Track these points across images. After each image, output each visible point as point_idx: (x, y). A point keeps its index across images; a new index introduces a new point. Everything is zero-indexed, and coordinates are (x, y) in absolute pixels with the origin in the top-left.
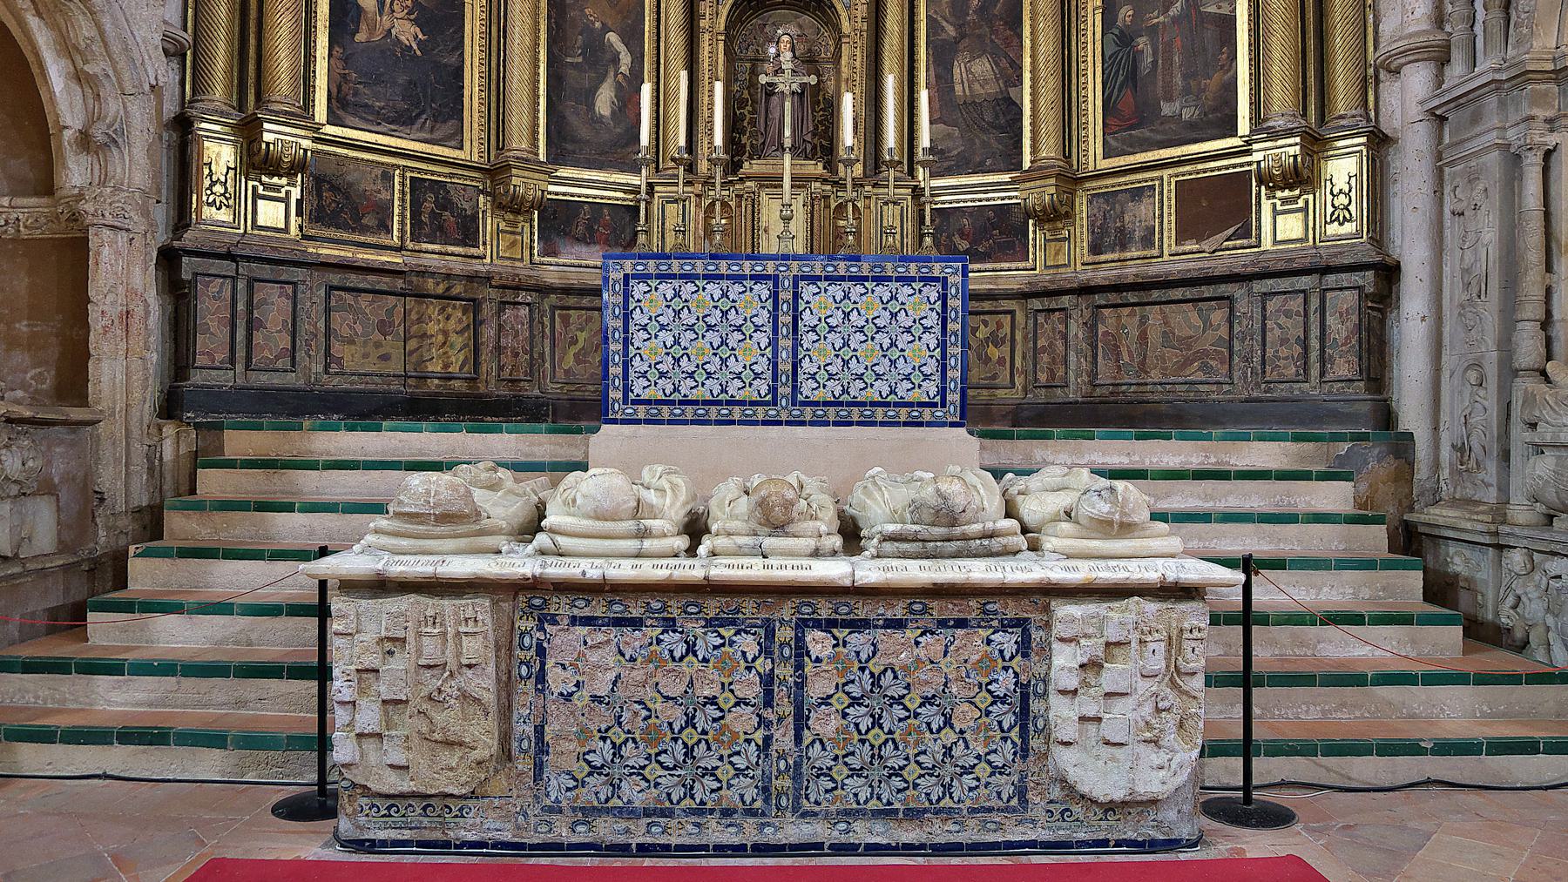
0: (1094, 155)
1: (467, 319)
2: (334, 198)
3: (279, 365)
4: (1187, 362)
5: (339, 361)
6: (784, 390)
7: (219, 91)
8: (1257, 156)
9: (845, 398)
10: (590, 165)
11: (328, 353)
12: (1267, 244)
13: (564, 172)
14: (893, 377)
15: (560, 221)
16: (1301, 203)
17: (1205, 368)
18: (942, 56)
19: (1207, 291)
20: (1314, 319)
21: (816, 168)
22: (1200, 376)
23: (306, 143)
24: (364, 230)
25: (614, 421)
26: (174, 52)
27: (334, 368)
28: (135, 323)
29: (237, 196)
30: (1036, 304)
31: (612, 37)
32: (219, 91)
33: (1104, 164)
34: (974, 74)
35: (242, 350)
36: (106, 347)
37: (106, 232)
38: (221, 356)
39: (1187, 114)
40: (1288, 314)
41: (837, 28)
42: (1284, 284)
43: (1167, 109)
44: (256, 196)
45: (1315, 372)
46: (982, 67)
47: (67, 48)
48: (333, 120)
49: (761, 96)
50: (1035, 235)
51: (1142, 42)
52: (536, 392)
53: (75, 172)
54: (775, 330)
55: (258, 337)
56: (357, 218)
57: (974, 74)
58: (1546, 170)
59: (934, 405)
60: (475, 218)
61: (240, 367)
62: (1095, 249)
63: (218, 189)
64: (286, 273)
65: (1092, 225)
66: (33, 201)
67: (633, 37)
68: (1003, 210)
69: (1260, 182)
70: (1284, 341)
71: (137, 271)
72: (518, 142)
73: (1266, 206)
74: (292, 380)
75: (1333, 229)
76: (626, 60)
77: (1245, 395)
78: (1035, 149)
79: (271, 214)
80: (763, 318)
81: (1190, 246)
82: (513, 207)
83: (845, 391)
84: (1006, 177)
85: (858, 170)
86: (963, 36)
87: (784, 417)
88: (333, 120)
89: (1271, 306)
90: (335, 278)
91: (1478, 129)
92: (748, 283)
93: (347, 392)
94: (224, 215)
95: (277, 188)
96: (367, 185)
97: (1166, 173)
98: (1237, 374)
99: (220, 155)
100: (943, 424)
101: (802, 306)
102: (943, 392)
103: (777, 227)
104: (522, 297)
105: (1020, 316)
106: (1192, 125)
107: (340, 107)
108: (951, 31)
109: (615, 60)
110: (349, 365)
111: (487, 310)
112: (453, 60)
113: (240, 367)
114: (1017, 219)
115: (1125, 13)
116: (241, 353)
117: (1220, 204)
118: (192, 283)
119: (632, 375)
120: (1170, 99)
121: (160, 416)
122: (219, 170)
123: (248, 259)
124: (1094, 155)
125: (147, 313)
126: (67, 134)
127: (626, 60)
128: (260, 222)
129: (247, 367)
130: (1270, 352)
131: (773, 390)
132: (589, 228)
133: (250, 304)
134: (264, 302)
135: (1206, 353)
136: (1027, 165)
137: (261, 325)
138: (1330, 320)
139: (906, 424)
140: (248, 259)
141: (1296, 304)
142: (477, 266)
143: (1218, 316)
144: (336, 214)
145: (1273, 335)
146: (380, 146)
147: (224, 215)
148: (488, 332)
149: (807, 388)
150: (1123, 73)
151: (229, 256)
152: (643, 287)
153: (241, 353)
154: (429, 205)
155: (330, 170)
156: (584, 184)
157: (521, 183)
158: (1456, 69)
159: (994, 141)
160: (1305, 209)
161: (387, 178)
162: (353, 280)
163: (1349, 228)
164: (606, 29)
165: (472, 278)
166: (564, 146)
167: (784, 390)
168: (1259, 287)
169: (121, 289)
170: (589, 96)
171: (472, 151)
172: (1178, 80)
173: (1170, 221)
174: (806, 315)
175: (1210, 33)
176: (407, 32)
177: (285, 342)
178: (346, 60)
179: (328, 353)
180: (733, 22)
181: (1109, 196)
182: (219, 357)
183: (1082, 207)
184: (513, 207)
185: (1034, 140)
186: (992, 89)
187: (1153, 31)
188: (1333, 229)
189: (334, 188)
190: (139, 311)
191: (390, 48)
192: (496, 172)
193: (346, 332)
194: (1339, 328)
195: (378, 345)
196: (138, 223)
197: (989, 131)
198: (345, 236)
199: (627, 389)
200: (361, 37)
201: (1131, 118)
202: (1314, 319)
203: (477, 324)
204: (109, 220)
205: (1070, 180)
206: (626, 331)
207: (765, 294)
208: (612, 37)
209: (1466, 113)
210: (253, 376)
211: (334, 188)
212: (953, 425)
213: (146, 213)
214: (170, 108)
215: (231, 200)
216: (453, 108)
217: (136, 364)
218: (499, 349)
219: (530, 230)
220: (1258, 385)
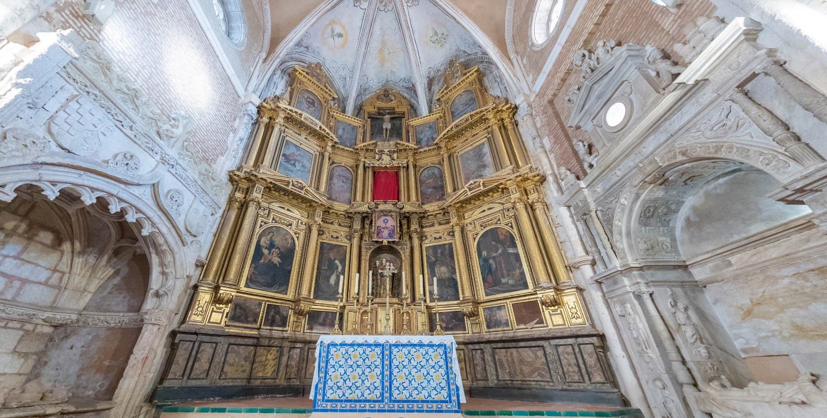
0: (482, 295)
1: (278, 355)
2: (241, 312)
3: (201, 376)
4: (533, 372)
5: (226, 374)
6: (387, 395)
7: (211, 277)
8: (540, 296)
9: (411, 398)
10: (326, 299)
11: (222, 370)
12: (551, 326)
13: (317, 301)
14: (429, 388)
15: (315, 318)
16: (559, 312)
17: (540, 375)
18: (432, 266)
19: (533, 343)
20: (579, 355)
21: (395, 300)
22: (539, 378)
23: (233, 294)
24: (248, 322)
25: (318, 411)
26: (199, 265)
27: (223, 377)
28: (148, 362)
29: (206, 311)
30: (471, 347)
31: (337, 262)
32: (211, 277)
33: (486, 298)
34: (442, 271)
35: (187, 372)
36: (130, 373)
37: (150, 326)
38: (179, 373)
39: (510, 282)
40: (568, 354)
41: (401, 259)
42: (562, 342)
43: (503, 281)
44: (213, 311)
45: (586, 378)
46: (444, 269)
47: (162, 264)
48: (247, 286)
49: (379, 277)
50: (468, 322)
51: (491, 261)
52: (298, 383)
53: (150, 303)
54: (383, 368)
55: (197, 365)
56: (246, 317)
57: (442, 271)
58: (653, 300)
59: (447, 402)
60: (286, 317)
61: (185, 378)
62: (488, 327)
63: (200, 309)
64: (215, 339)
65: (486, 319)
66: (132, 314)
67: (343, 262)
68: (455, 314)
69: (543, 304)
70: (570, 365)
71: (157, 341)
72: (304, 293)
73: (546, 312)
74: (205, 383)
75: (573, 321)
76: (340, 268)
77: (560, 388)
78: (463, 294)
79: (216, 317)
80: (378, 362)
81: (522, 326)
82: (299, 313)
83: (411, 395)
84: (456, 302)
85: (409, 301)
86: (437, 260)
87: (386, 408)
88: (247, 286)
89: (560, 349)
90: (232, 340)
91: (617, 286)
92: (373, 348)
93: (225, 387)
94: (199, 319)
95: (220, 308)
96: (253, 307)
97: (508, 301)
98: (554, 378)
99: (205, 297)
100: (451, 412)
101: (393, 378)
102: (449, 395)
103: (384, 322)
104: (298, 345)
105: (466, 351)
106: (513, 286)
107: (250, 282)
108: (433, 259)
109: (337, 268)
110: (229, 375)
111: (286, 350)
112: (289, 268)
113: (185, 378)
114: (460, 316)
115: (484, 253)
116: (188, 372)
117: (529, 311)
118: (178, 344)
119: (327, 388)
120: (503, 277)
121: (145, 401)
122: (202, 303)
123: (203, 334)
124: (482, 295)
125: (155, 357)
126: (151, 291)
127: (340, 268)
128: (211, 320)
129: (188, 378)
130: (565, 370)
131: (382, 395)
132: (324, 320)
133: (197, 352)
134: (203, 351)
135: (539, 368)
136: (461, 299)
137: (200, 360)
138: (585, 356)
139: (436, 411)
140: (203, 334)
141: (570, 349)
142: (285, 334)
143: (540, 353)
144: (239, 317)
145: (564, 362)
146: (261, 296)
147: (199, 319)
148: (285, 359)
149: (395, 393)
150: (487, 270)
151: (196, 334)
152: (334, 349)
153: (188, 372)
154: (272, 313)
155: (241, 302)
156: (321, 305)
157: (303, 306)
158: (600, 267)
159: (451, 291)
160: (561, 313)
161: (260, 304)
162: (240, 341)
163: (580, 321)
164: (335, 259)
165: (283, 338)
166: (319, 292)
167: (387, 395)
168: (554, 342)
169: (148, 348)
170: (328, 279)
171: (290, 295)
172: (505, 271)
173: (513, 317)
174: (394, 361)
175: (512, 259)
176: (276, 260)
177: (206, 366)
178: (255, 268)
179: (222, 370)
180: (371, 258)
181: (490, 309)
182: (178, 374)
183: (481, 310)
184: (299, 313)
185: (463, 290)
186: (447, 275)
187: (494, 258)
188: (573, 321)
189: (241, 308)
190: (151, 356)
191: (271, 265)
192: (296, 301)
193: (231, 361)
194: (591, 361)
195: (242, 366)
196: (164, 321)
197: (450, 288)
198: (241, 325)
199: (324, 395)
200: (261, 261)
201: (492, 281)
202: (579, 355)
203: (281, 355)
204: (153, 321)
205: (476, 303)
206: (326, 367)
207: (379, 352)
208: (337, 262)
209: (610, 281)
210: (189, 381)
211: (241, 308)
212: (456, 412)
213: (169, 318)
214: (193, 283)
215: (203, 313)
216: (286, 283)
217: (142, 379)
218: (287, 366)
219: (304, 321)
220: (564, 383)
